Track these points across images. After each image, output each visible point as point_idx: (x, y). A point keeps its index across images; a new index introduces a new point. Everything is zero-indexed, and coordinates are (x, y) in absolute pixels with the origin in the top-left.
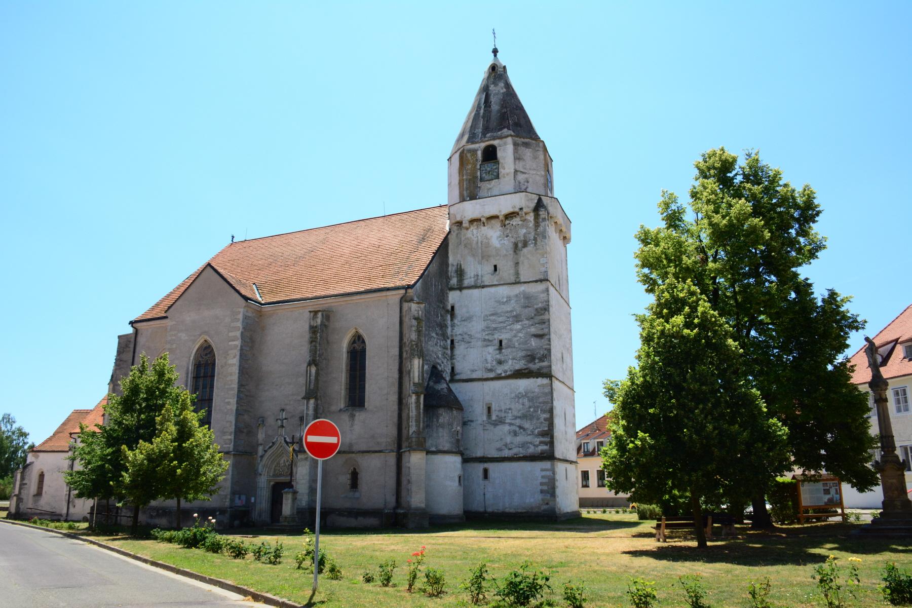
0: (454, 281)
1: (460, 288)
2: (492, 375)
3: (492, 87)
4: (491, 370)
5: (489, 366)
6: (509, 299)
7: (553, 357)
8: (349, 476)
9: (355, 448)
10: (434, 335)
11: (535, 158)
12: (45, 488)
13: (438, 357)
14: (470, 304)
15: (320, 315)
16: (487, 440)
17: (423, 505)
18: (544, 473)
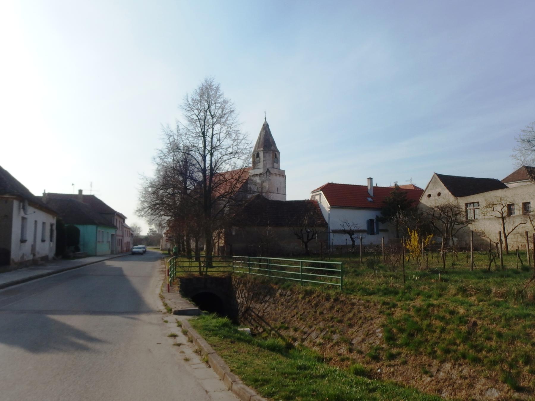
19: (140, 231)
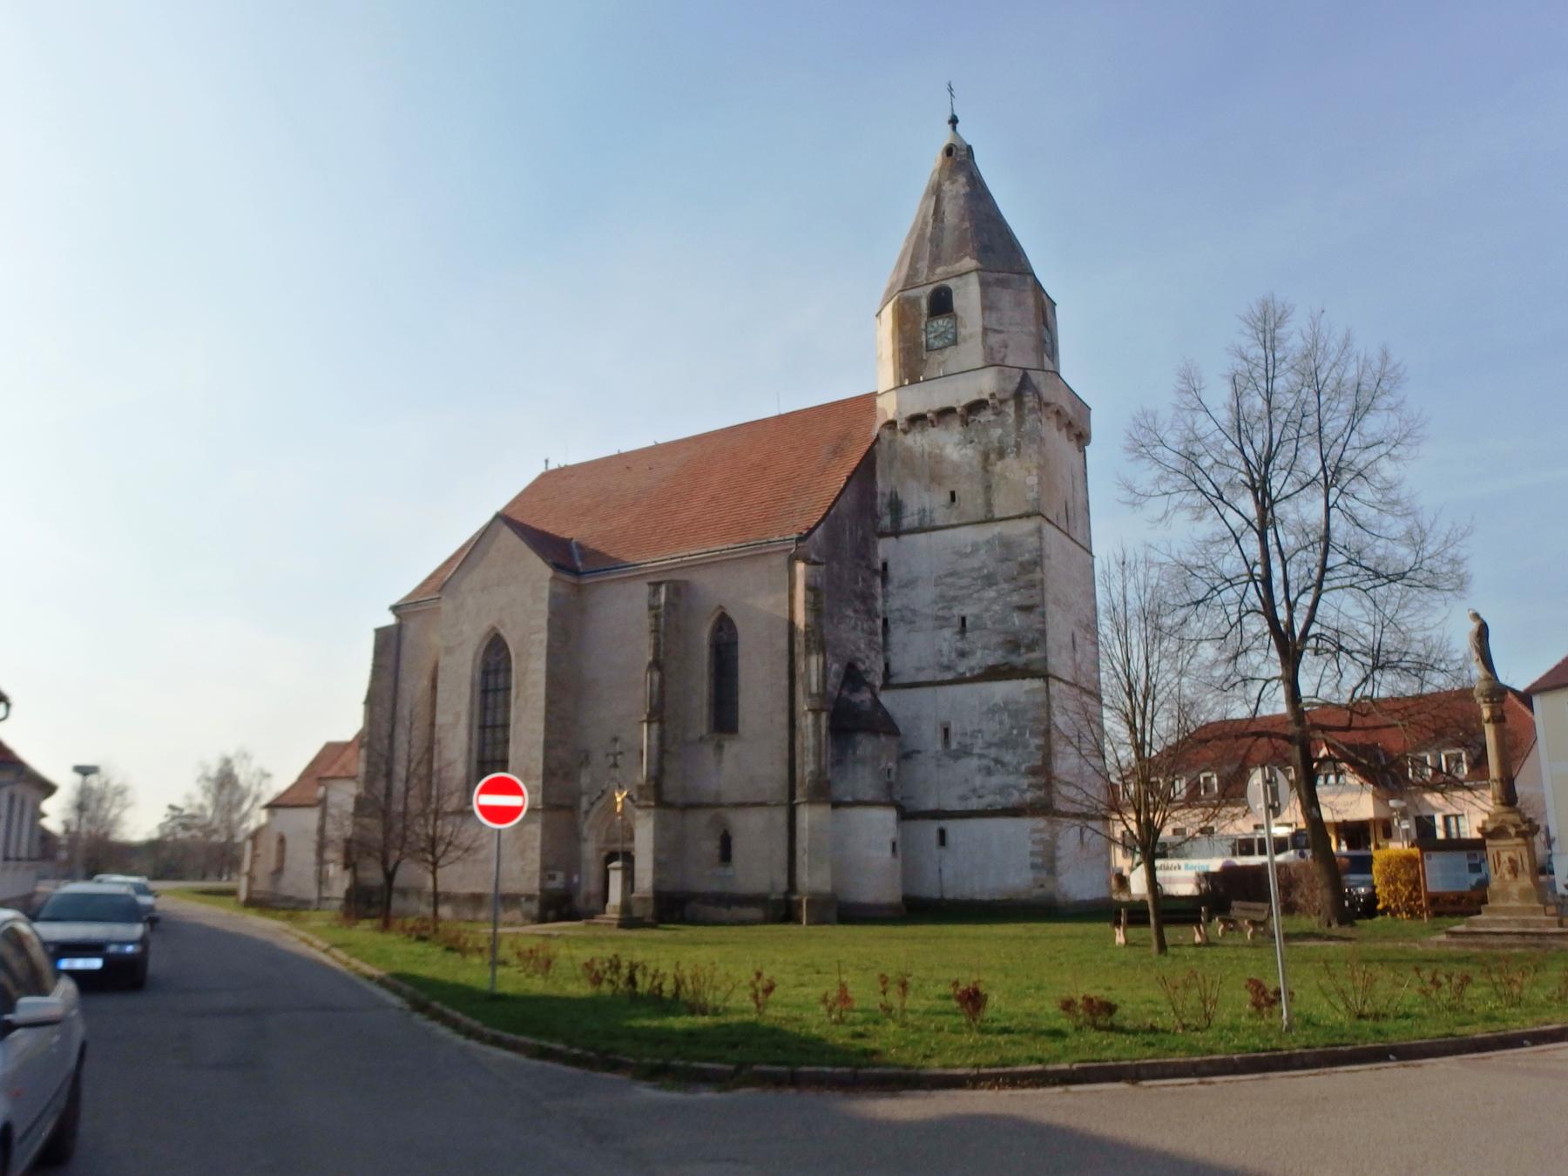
0: (886, 521)
1: (897, 532)
2: (949, 676)
3: (947, 186)
4: (948, 668)
5: (945, 661)
6: (976, 548)
7: (1050, 643)
8: (717, 843)
9: (725, 799)
10: (850, 612)
11: (1019, 304)
12: (288, 863)
13: (858, 649)
14: (915, 559)
15: (663, 589)
16: (943, 785)
17: (827, 888)
18: (1037, 836)
19: (124, 807)
